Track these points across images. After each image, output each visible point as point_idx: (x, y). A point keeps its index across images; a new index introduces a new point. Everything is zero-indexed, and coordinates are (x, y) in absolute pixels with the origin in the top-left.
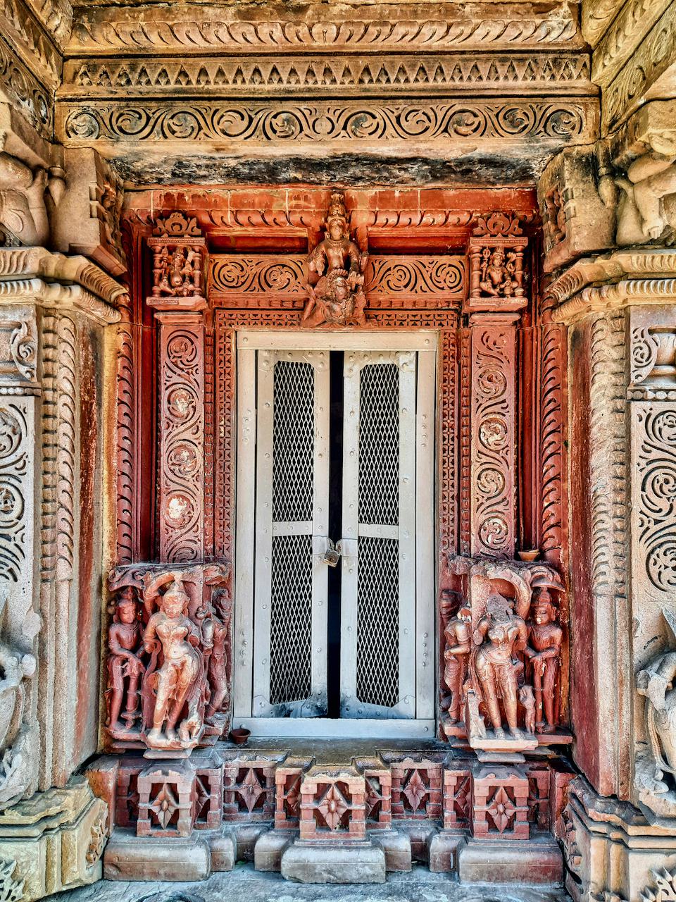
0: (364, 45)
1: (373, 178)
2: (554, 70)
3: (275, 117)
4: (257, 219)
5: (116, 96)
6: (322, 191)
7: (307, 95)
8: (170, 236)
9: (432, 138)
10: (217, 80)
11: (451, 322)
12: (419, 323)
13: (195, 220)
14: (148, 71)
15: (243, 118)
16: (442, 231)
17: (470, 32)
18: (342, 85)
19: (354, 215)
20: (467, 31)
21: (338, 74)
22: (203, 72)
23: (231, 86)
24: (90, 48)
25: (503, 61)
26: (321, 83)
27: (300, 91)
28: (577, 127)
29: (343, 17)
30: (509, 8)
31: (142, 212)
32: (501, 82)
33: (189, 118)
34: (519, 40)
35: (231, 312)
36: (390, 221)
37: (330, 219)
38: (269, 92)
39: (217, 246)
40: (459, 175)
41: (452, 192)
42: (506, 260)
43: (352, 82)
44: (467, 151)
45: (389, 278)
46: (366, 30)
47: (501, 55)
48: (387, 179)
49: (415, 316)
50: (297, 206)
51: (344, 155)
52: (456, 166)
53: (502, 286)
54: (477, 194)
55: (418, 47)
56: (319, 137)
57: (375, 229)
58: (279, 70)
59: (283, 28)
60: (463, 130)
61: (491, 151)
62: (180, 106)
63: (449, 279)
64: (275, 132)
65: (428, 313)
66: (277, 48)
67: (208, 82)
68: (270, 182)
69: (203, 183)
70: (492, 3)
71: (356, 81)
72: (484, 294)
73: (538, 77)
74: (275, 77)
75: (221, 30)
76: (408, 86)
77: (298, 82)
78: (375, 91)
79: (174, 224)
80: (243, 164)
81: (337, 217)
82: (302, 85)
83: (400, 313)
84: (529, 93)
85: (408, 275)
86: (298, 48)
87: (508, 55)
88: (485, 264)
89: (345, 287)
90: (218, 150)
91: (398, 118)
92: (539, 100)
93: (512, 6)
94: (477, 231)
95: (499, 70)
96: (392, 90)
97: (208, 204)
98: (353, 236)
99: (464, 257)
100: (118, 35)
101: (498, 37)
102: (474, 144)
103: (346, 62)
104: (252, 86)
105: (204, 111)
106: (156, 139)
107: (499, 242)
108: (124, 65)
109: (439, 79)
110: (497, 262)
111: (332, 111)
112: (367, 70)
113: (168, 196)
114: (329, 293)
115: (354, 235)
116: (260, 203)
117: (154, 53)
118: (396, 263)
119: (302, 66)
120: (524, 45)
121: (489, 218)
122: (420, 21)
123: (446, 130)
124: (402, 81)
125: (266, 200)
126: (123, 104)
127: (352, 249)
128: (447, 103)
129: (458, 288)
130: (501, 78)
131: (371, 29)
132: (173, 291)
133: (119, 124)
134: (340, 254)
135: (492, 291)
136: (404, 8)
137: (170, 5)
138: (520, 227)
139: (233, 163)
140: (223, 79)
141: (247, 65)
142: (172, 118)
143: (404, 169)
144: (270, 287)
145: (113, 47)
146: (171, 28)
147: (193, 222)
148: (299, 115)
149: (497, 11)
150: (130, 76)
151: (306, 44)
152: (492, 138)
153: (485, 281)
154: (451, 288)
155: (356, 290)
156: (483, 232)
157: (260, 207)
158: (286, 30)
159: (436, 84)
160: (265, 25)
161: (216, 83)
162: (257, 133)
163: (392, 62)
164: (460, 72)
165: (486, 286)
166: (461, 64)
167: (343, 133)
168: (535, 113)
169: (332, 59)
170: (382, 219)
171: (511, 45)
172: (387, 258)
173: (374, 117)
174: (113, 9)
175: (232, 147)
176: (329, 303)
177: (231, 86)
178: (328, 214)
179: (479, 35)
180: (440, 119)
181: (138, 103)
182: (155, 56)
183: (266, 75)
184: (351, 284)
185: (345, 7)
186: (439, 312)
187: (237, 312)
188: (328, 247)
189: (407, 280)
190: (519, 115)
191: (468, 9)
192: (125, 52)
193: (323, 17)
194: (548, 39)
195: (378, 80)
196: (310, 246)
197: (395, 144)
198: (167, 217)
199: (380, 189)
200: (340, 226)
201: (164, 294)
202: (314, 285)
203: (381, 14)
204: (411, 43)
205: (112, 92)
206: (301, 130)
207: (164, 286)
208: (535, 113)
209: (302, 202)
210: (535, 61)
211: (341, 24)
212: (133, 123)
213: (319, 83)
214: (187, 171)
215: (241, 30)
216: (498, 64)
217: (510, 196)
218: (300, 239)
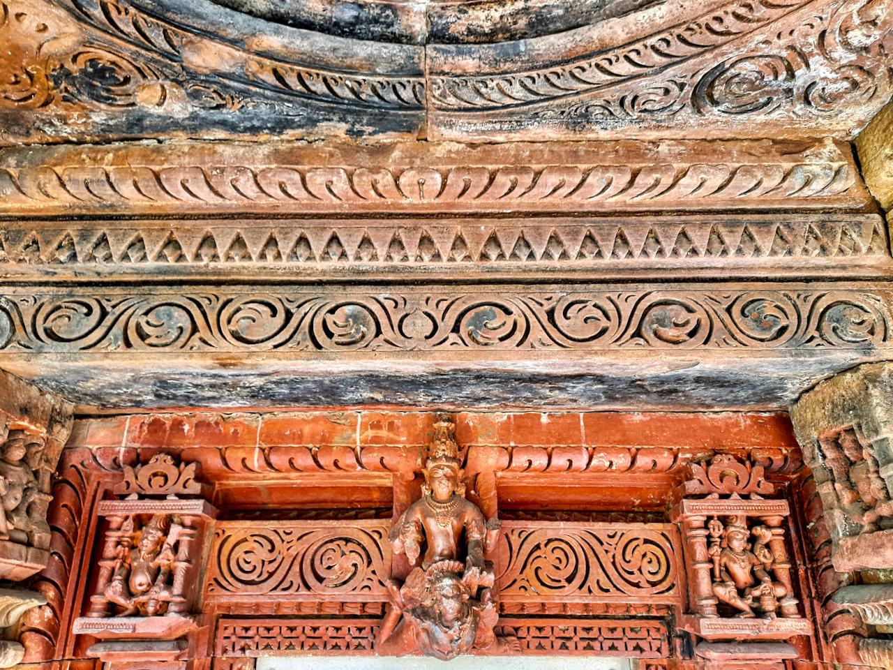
0: (490, 202)
1: (505, 399)
2: (825, 240)
3: (332, 311)
4: (304, 461)
5: (55, 279)
6: (420, 415)
7: (390, 277)
8: (142, 497)
9: (614, 347)
10: (232, 253)
11: (656, 644)
12: (596, 645)
13: (193, 466)
14: (110, 240)
15: (274, 312)
16: (626, 481)
17: (671, 181)
18: (450, 263)
19: (472, 453)
20: (667, 180)
21: (445, 248)
22: (208, 241)
23: (255, 263)
24: (18, 205)
25: (731, 225)
26: (414, 260)
27: (378, 271)
28: (879, 330)
29: (453, 161)
30: (735, 149)
31: (105, 451)
32: (731, 259)
33: (177, 313)
34: (755, 194)
35: (246, 623)
36: (535, 464)
37: (430, 465)
38: (324, 272)
39: (230, 507)
40: (655, 396)
41: (638, 418)
42: (753, 540)
43: (468, 258)
44: (678, 367)
45: (538, 563)
46: (492, 180)
47: (725, 217)
48: (528, 400)
49: (588, 630)
50: (376, 439)
51: (455, 371)
52: (651, 385)
53: (757, 593)
54: (680, 420)
55: (581, 206)
56: (409, 344)
57: (508, 474)
58: (342, 240)
59: (350, 177)
60: (671, 333)
61: (721, 367)
62: (165, 294)
63: (647, 568)
64: (330, 335)
65: (612, 624)
66: (341, 206)
67: (215, 257)
68: (329, 403)
69: (214, 405)
70: (705, 140)
71: (476, 257)
72: (726, 610)
73: (798, 250)
74: (334, 249)
75: (242, 179)
76: (565, 264)
77: (374, 257)
78: (508, 271)
79: (155, 475)
80: (277, 383)
81: (443, 462)
82: (381, 263)
83: (561, 625)
84: (778, 274)
85: (572, 560)
86: (377, 206)
87: (739, 217)
88: (715, 550)
89: (458, 597)
90: (224, 366)
91: (551, 313)
92: (801, 285)
93: (739, 144)
94: (692, 486)
95: (727, 240)
96: (538, 270)
97: (223, 438)
98: (471, 491)
99: (669, 526)
100: (63, 185)
101: (721, 188)
102: (695, 358)
103: (457, 227)
104: (293, 263)
105: (204, 303)
106: (111, 348)
107: (736, 508)
108: (72, 229)
109: (622, 254)
110: (738, 544)
111: (433, 303)
112: (493, 240)
113: (156, 425)
114: (428, 603)
115: (472, 483)
116: (312, 436)
117: (127, 213)
118: (551, 535)
119: (382, 233)
120: (764, 201)
121: (709, 463)
122: (583, 167)
123: (638, 334)
124: (557, 256)
125: (321, 428)
126: (64, 290)
127: (471, 515)
128: (637, 290)
129: (665, 585)
130: (732, 251)
131: (500, 178)
132: (129, 604)
133: (48, 324)
134: (449, 528)
135: (740, 604)
136: (556, 148)
137: (160, 142)
138: (767, 478)
139: (259, 382)
140: (242, 253)
141: (285, 233)
142: (146, 314)
143: (559, 389)
144: (320, 579)
145: (56, 203)
146: (157, 176)
147: (190, 471)
148: (375, 308)
149: (714, 151)
150: (77, 248)
151: (389, 201)
152: (725, 348)
153: (722, 582)
154: (653, 584)
155: (477, 598)
156: (703, 489)
157: (311, 442)
158: (355, 179)
159: (615, 261)
160: (318, 172)
161: (228, 258)
162: (298, 337)
163: (537, 228)
164: (658, 242)
165: (727, 593)
166: (658, 230)
167: (453, 337)
168: (795, 306)
169: (434, 222)
170: (520, 460)
171: (742, 201)
172: (532, 525)
173: (508, 312)
174: (62, 148)
175: (249, 362)
176: (427, 624)
177: (255, 263)
178: (427, 455)
179: (687, 186)
180: (626, 315)
181: (90, 290)
182: (131, 218)
183: (318, 246)
184: (469, 586)
185: (456, 147)
186: (633, 623)
187: (259, 623)
188: (426, 515)
189: (571, 568)
190: (770, 310)
191: (663, 148)
192: (77, 211)
193: (418, 162)
194: (807, 192)
195: (514, 255)
196: (396, 505)
197: (547, 356)
198: (145, 462)
199: (517, 412)
200: (448, 478)
201: (112, 610)
202: (400, 581)
203: (515, 156)
204: (568, 200)
205: (47, 273)
206: (379, 332)
207: (113, 592)
208: (795, 306)
209: (384, 433)
210: (788, 226)
211: (449, 171)
212: (74, 322)
213: (412, 259)
214: (181, 392)
215: (278, 179)
216: (723, 231)
217: (737, 424)
218: (381, 489)
